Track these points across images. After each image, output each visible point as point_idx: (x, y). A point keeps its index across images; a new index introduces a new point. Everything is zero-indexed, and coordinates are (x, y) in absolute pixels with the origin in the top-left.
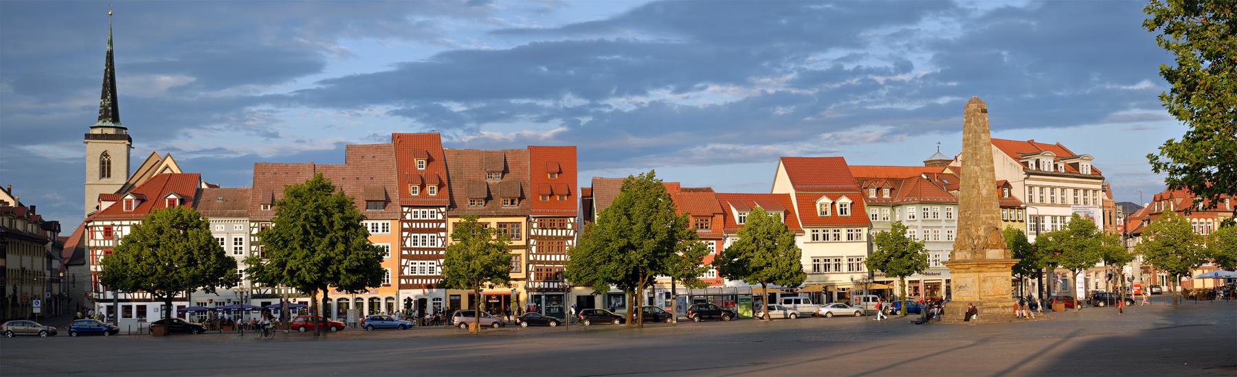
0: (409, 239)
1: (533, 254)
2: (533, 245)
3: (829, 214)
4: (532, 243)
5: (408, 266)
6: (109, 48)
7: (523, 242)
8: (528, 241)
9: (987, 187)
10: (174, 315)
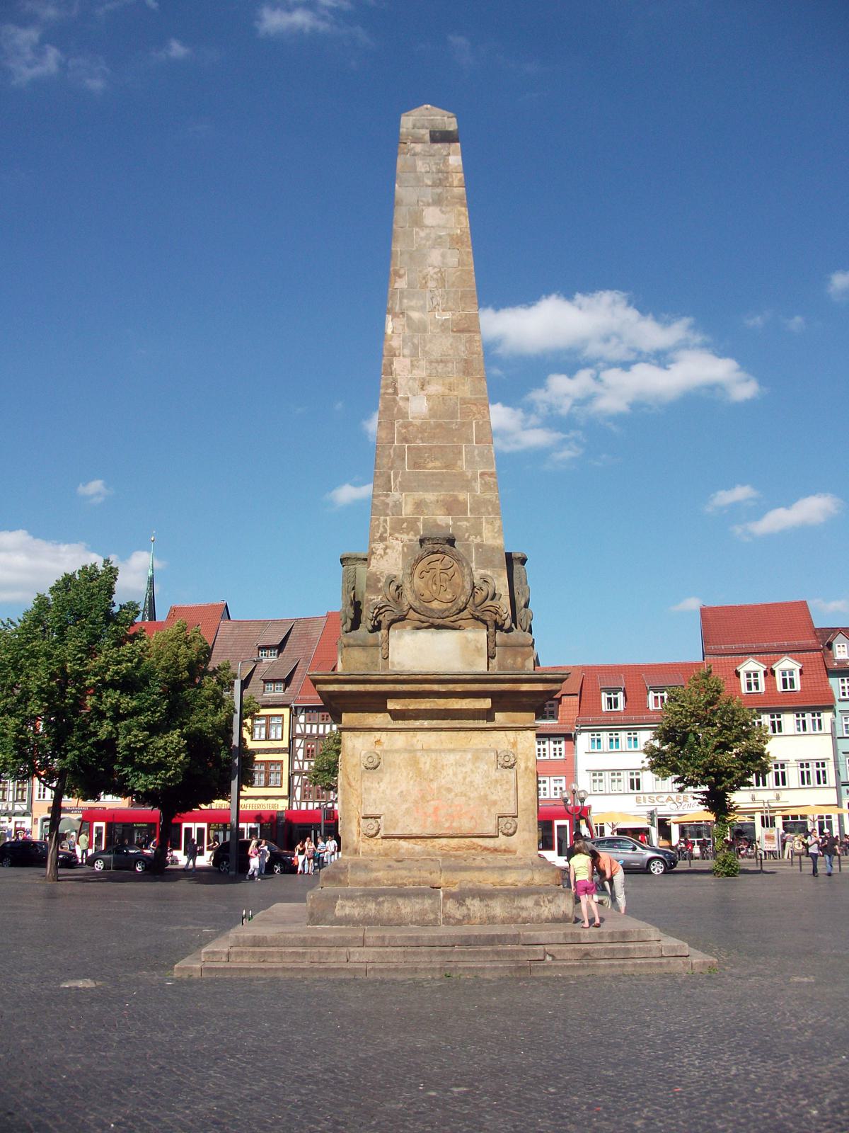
1: (299, 761)
2: (299, 748)
3: (762, 688)
4: (297, 745)
6: (150, 573)
7: (285, 744)
8: (291, 741)
9: (435, 388)
10: (780, 688)
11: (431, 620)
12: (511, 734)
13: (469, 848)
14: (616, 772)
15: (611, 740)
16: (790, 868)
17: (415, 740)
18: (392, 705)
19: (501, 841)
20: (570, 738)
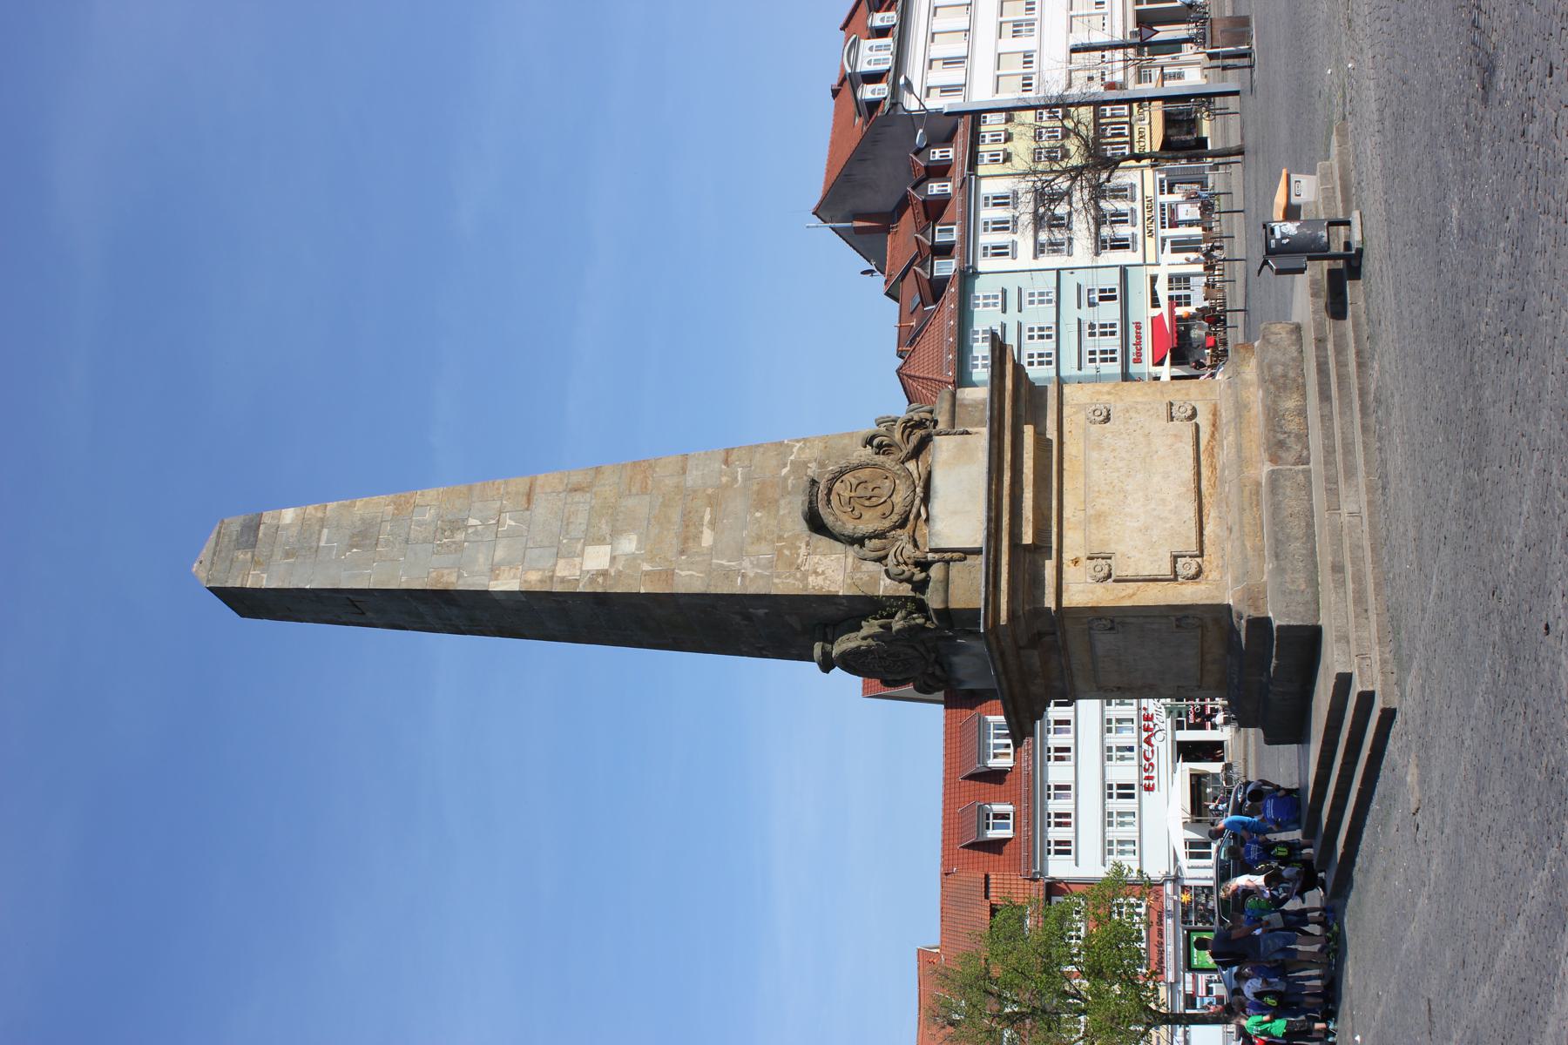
11: (917, 502)
13: (1212, 455)
14: (1107, 819)
15: (1057, 759)
16: (1236, 239)
17: (1073, 519)
20: (1054, 888)
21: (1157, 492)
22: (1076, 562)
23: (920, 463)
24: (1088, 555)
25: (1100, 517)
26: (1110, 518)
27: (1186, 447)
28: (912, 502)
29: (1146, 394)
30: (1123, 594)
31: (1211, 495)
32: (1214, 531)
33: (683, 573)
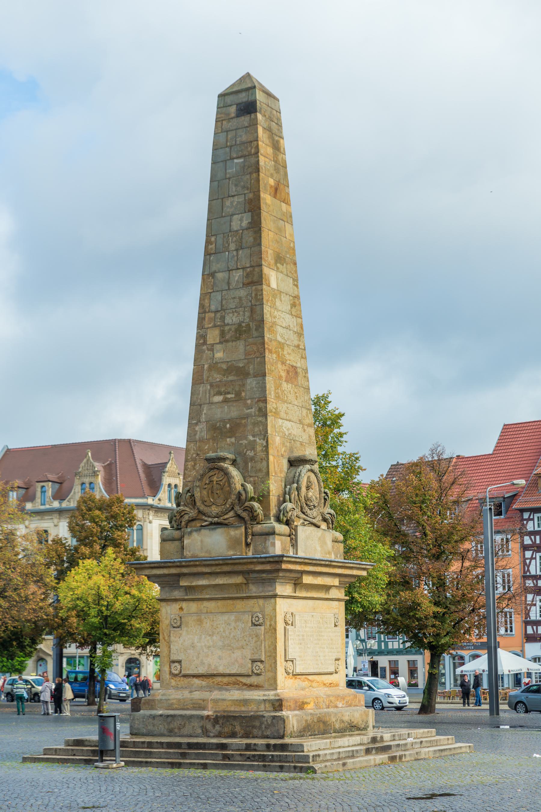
0: (533, 561)
5: (535, 605)
12: (261, 601)
17: (202, 606)
18: (184, 583)
19: (254, 680)
21: (212, 653)
22: (181, 609)
23: (234, 518)
24: (294, 613)
25: (200, 622)
26: (199, 627)
27: (235, 670)
28: (209, 517)
29: (269, 647)
30: (165, 634)
31: (213, 682)
32: (195, 683)
33: (201, 389)
